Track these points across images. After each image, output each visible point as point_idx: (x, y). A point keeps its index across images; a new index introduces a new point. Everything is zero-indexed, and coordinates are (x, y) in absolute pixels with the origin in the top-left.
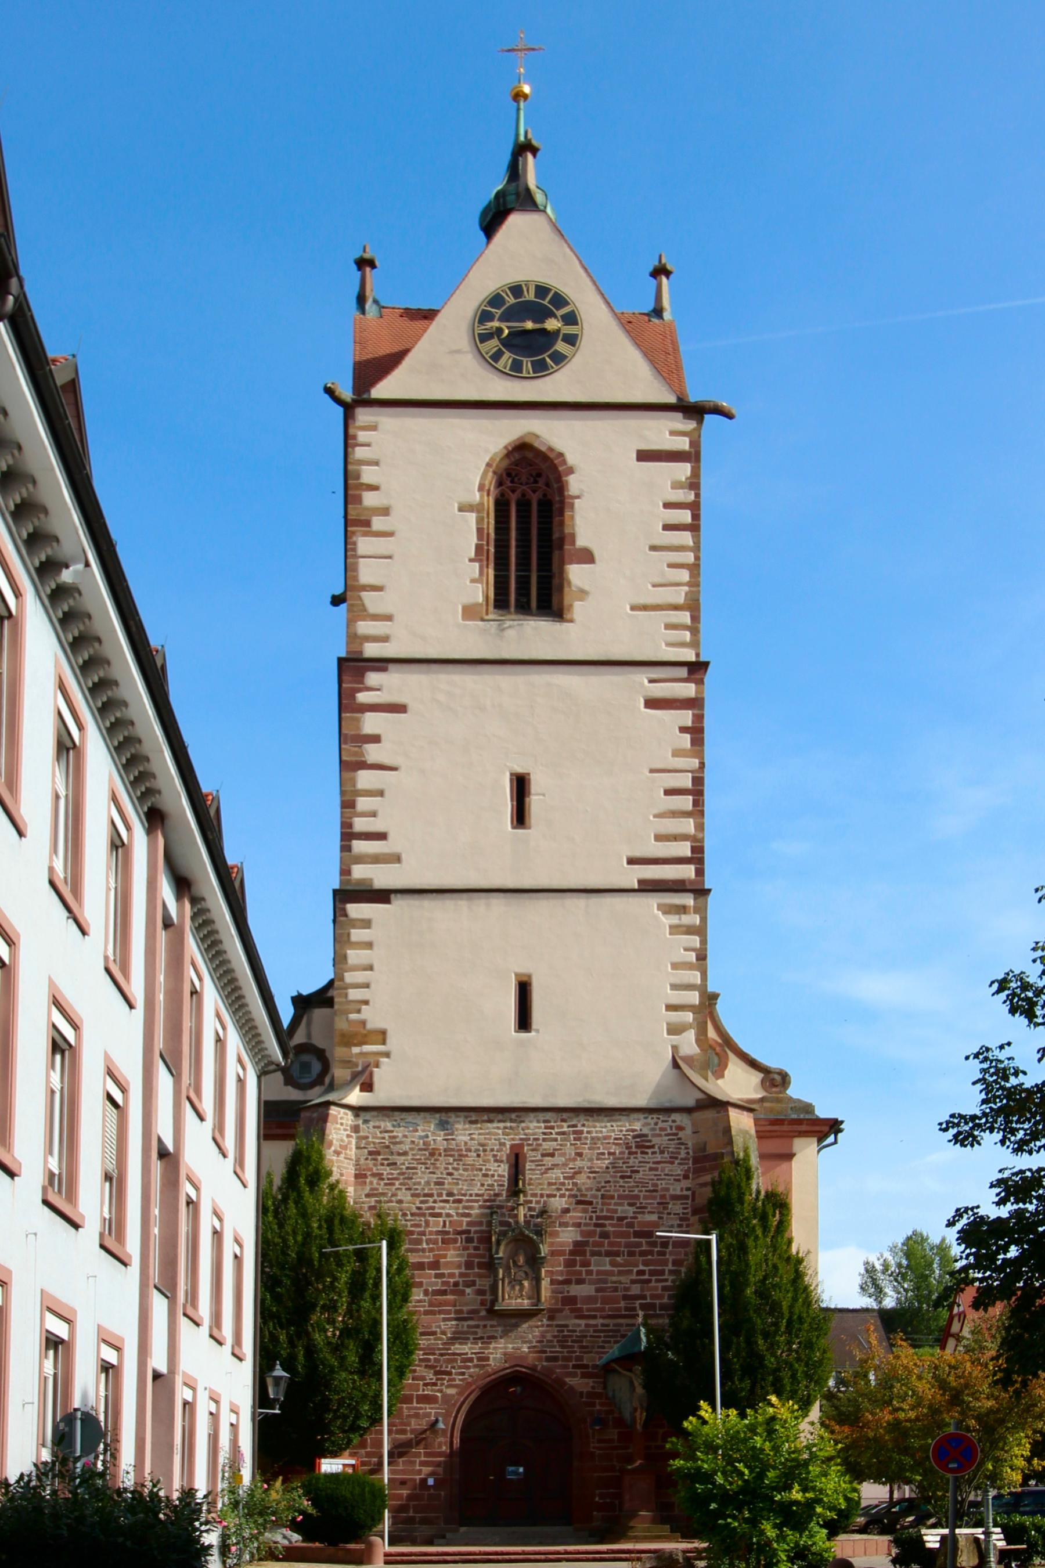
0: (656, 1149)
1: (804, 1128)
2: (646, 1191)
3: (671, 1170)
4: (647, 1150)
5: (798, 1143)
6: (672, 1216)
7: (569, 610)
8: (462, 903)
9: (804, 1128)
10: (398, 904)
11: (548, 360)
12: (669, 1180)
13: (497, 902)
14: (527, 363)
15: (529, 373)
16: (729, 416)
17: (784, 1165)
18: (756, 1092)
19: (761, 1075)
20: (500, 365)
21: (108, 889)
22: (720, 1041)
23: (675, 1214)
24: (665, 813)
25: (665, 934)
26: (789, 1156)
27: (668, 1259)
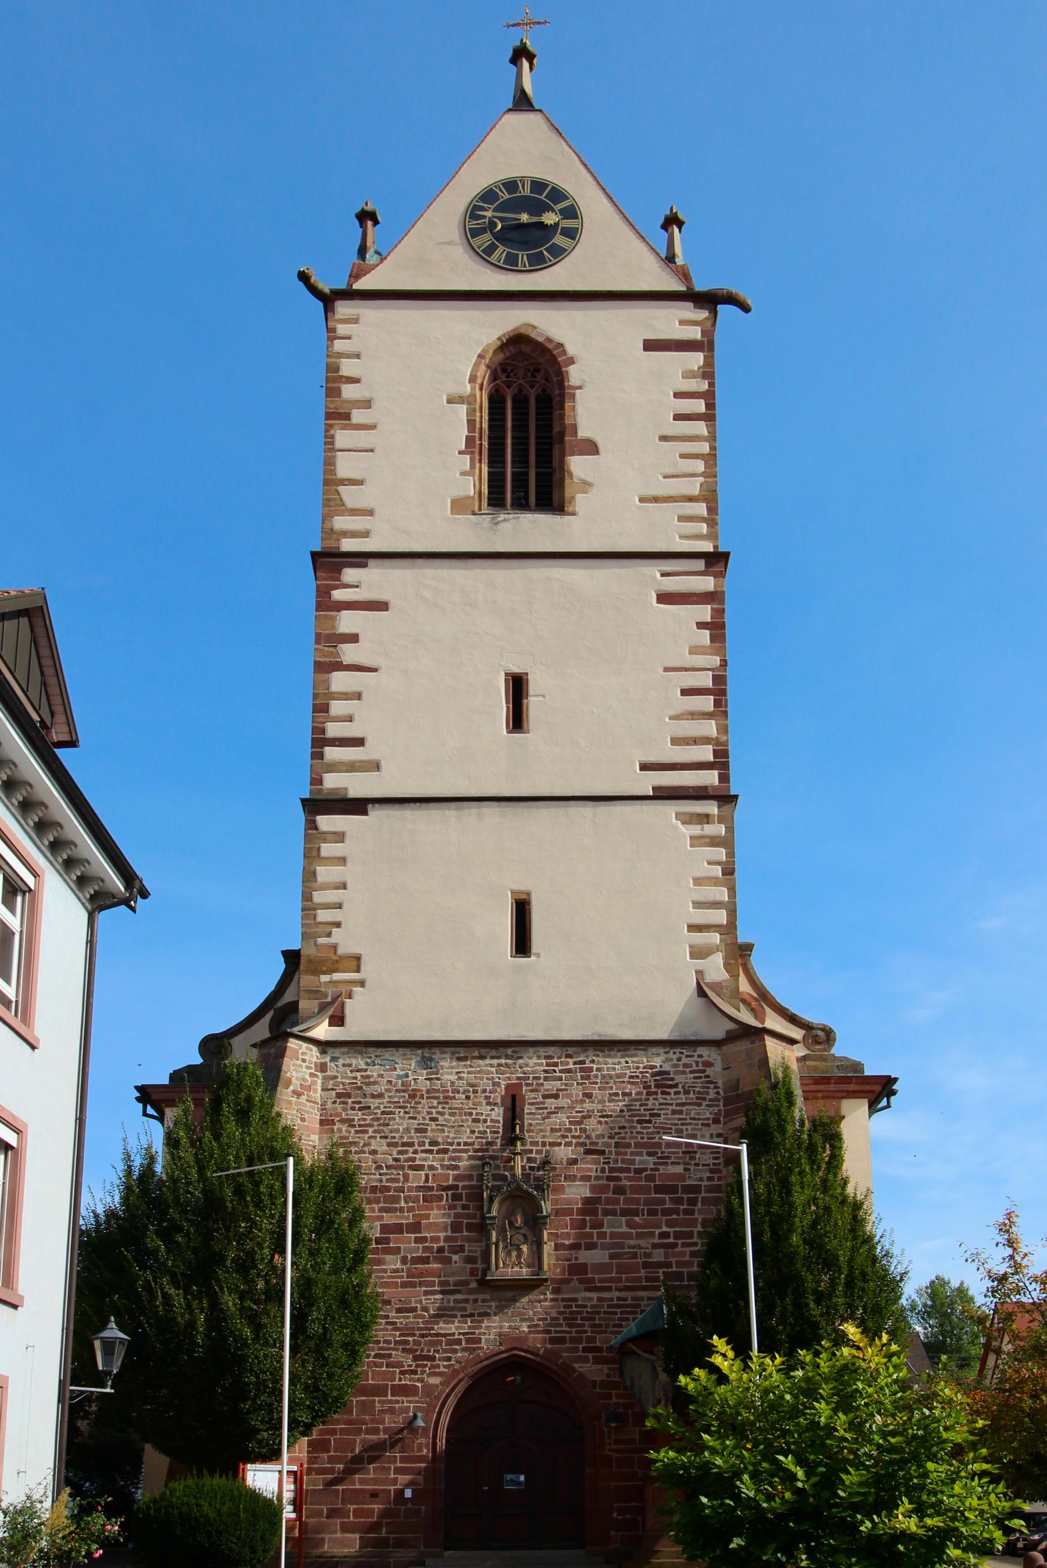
3: (698, 1114)
8: (450, 813)
9: (852, 1087)
10: (376, 814)
11: (545, 253)
13: (490, 811)
14: (523, 256)
15: (525, 266)
16: (746, 309)
20: (493, 258)
24: (682, 714)
25: (685, 847)
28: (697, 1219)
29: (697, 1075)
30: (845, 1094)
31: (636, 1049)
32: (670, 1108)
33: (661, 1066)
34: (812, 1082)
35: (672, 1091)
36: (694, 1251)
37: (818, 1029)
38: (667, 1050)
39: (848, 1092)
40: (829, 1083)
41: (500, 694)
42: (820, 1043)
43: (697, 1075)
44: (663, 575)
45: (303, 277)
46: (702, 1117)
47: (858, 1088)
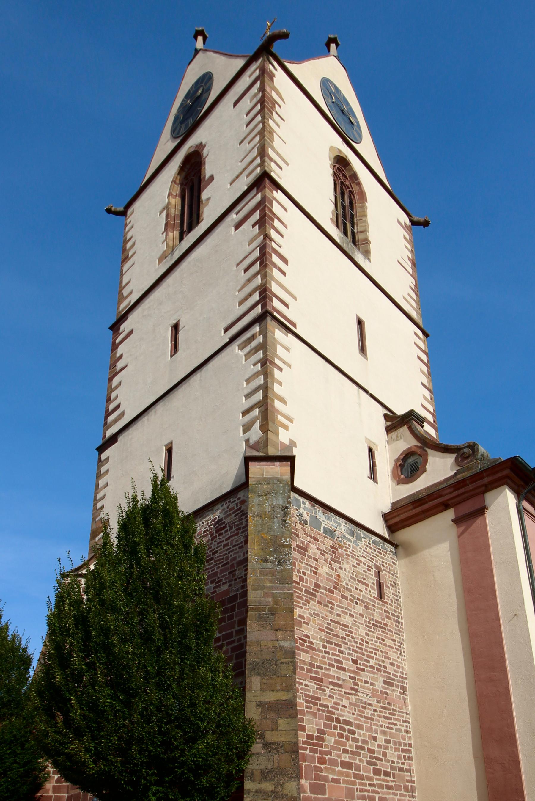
0: (228, 528)
1: (486, 480)
2: (222, 566)
3: (237, 541)
4: (222, 532)
5: (489, 496)
6: (238, 580)
7: (201, 216)
8: (145, 419)
9: (486, 480)
10: (120, 439)
12: (236, 549)
13: (159, 407)
16: (285, 36)
17: (479, 521)
18: (452, 470)
19: (454, 456)
21: (527, 566)
22: (420, 445)
23: (239, 578)
24: (245, 284)
25: (242, 362)
26: (481, 511)
27: (235, 620)
28: (235, 620)
29: (236, 513)
30: (484, 488)
31: (207, 512)
32: (222, 544)
33: (219, 517)
34: (452, 489)
35: (223, 531)
36: (234, 647)
37: (465, 448)
38: (222, 504)
39: (486, 485)
40: (466, 485)
41: (168, 340)
42: (467, 457)
43: (236, 513)
44: (237, 214)
45: (109, 211)
46: (239, 543)
47: (490, 478)
